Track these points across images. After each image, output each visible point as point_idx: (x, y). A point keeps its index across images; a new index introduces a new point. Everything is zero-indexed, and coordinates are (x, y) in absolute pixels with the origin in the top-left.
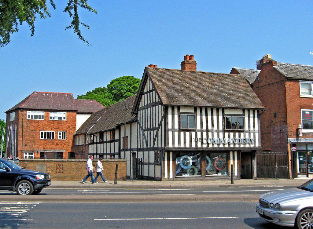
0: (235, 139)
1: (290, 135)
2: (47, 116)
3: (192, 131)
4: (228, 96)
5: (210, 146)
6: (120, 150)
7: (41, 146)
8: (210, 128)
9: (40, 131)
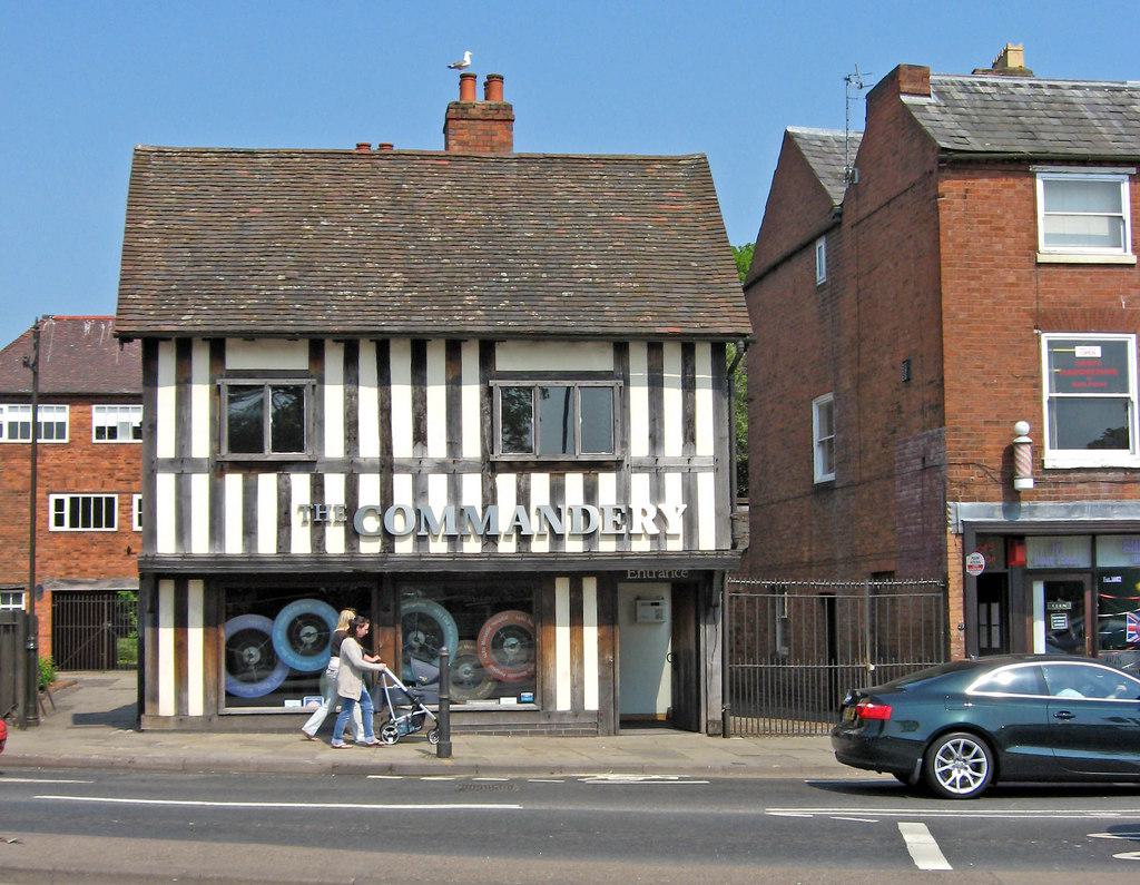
0: (559, 512)
1: (964, 485)
2: (81, 425)
3: (294, 467)
4: (546, 270)
5: (404, 548)
7: (57, 564)
8: (403, 447)
9: (49, 493)
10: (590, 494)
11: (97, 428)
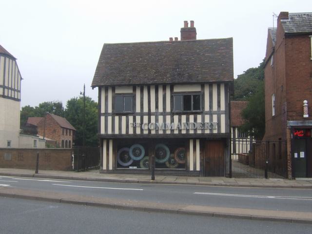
8: (153, 110)
10: (195, 120)
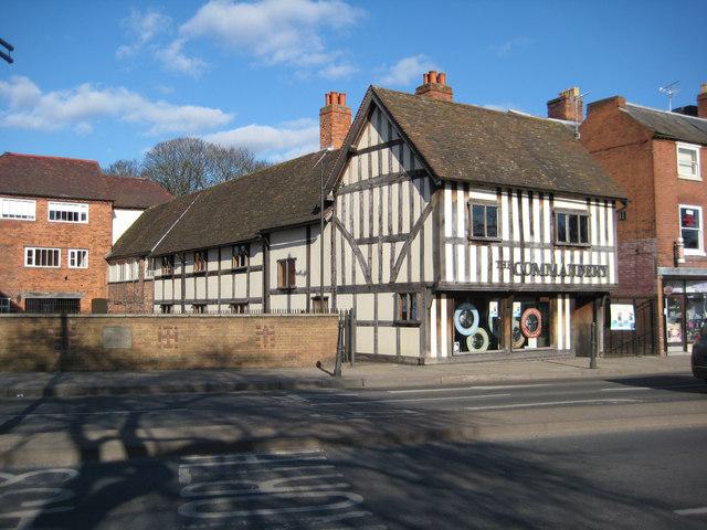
6: (267, 292)
8: (527, 238)
11: (585, 219)
